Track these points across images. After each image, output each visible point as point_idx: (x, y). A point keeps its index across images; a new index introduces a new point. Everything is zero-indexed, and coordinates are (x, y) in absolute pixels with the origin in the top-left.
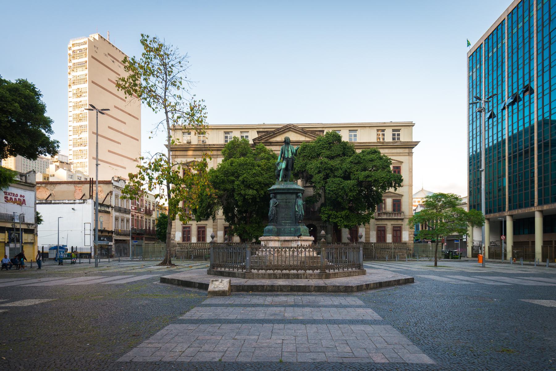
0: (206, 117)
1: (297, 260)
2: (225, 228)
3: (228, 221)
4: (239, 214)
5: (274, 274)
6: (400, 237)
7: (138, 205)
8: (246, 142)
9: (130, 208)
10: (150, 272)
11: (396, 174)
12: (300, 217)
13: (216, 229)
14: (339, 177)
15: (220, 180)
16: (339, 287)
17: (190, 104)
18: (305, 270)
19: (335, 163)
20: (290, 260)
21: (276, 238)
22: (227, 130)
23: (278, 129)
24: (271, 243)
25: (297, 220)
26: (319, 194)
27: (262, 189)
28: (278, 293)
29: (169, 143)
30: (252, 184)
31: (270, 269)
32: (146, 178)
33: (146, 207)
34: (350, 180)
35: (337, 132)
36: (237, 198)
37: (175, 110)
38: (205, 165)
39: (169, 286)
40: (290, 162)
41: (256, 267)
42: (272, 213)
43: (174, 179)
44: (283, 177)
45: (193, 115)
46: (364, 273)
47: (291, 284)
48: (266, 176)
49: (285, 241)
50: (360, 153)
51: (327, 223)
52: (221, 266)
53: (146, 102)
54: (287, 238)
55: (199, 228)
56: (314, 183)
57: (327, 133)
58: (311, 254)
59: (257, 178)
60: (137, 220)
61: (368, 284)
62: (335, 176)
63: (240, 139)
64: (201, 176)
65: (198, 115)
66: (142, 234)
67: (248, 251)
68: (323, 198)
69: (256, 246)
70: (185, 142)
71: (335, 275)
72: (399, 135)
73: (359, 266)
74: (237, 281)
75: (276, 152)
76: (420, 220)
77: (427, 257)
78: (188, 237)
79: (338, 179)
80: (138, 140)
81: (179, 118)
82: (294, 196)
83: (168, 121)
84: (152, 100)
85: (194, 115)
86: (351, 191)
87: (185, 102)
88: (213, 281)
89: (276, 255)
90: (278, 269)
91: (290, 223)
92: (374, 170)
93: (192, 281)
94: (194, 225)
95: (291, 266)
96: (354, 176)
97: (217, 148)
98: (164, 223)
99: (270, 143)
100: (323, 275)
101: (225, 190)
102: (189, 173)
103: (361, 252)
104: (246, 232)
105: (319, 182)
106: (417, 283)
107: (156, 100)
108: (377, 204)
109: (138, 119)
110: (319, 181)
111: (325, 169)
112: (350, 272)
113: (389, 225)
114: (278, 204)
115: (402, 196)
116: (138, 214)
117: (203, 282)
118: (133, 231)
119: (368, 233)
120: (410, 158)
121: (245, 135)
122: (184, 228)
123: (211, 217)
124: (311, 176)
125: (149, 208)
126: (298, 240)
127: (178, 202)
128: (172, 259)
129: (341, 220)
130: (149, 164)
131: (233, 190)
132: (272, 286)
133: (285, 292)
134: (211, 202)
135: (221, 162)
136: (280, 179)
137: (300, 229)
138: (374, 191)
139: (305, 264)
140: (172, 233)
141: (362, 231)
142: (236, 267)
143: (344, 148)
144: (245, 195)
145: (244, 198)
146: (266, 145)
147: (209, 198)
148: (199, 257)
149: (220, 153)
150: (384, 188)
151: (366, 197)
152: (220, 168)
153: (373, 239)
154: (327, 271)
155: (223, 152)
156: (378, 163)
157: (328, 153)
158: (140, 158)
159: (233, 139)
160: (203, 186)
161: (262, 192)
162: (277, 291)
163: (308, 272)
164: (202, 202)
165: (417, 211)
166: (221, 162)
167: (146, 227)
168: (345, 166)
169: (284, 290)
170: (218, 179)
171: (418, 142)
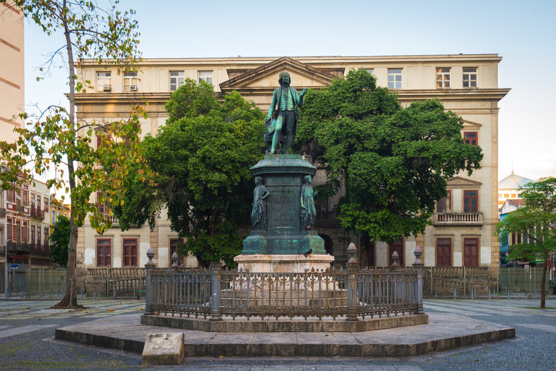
0: (138, 42)
1: (306, 298)
2: (172, 241)
3: (177, 230)
4: (198, 217)
5: (264, 324)
6: (477, 257)
7: (19, 201)
8: (207, 88)
9: (5, 207)
10: (39, 320)
11: (471, 146)
12: (308, 219)
13: (156, 242)
14: (371, 150)
15: (165, 157)
16: (383, 346)
17: (109, 18)
18: (320, 316)
19: (365, 125)
20: (291, 298)
21: (266, 257)
22: (174, 68)
23: (264, 66)
24: (257, 268)
25: (302, 225)
26: (336, 180)
27: (237, 172)
28: (272, 359)
29: (72, 88)
30: (219, 163)
31: (255, 315)
32: (32, 149)
33: (33, 206)
34: (392, 155)
35: (368, 71)
36: (192, 188)
37: (83, 29)
38: (136, 127)
39: (70, 346)
40: (290, 118)
41: (230, 312)
42: (258, 211)
43: (81, 154)
44: (277, 147)
45: (115, 38)
46: (424, 321)
47: (295, 342)
48: (244, 148)
49: (281, 262)
50: (408, 109)
51: (351, 232)
52: (166, 310)
53: (30, 15)
54: (286, 257)
55: (125, 241)
56: (327, 161)
57: (350, 72)
58: (331, 287)
59: (228, 151)
60: (17, 228)
61: (437, 342)
62: (365, 149)
63: (198, 84)
64: (129, 147)
65: (124, 38)
66: (27, 253)
67: (216, 280)
68: (343, 188)
69: (227, 272)
70: (101, 89)
71: (374, 325)
72: (474, 77)
73: (416, 309)
74: (196, 337)
75: (261, 107)
76: (517, 225)
77: (523, 291)
78: (106, 258)
79: (370, 154)
80: (18, 87)
81: (89, 42)
82: (298, 181)
83: (69, 49)
84: (41, 12)
85: (116, 38)
86: (393, 175)
87: (101, 14)
88: (151, 337)
89: (266, 288)
90: (270, 315)
91: (290, 230)
92: (433, 139)
93: (113, 336)
94: (117, 237)
95: (294, 308)
96: (398, 149)
97: (158, 100)
98: (65, 232)
100: (352, 324)
101: (171, 173)
102: (108, 142)
103: (420, 283)
104: (209, 248)
105: (337, 160)
106: (520, 338)
107: (48, 12)
108: (438, 198)
109: (18, 50)
110: (336, 157)
111: (347, 137)
112: (401, 319)
113: (458, 237)
114: (269, 196)
115: (480, 184)
116: (19, 217)
117: (134, 339)
118: (11, 248)
119: (419, 250)
120: (494, 118)
121: (204, 76)
122: (99, 241)
123: (147, 223)
124: (323, 150)
125: (39, 207)
126: (305, 262)
127: (88, 194)
128: (78, 296)
129: (375, 228)
130: (37, 125)
131: (186, 174)
132: (261, 346)
133: (284, 356)
134: (147, 195)
135: (164, 125)
136: (273, 150)
137: (308, 241)
138: (431, 176)
139: (319, 304)
140: (78, 250)
141: (410, 246)
142: (193, 311)
143: (381, 100)
144: (208, 182)
145: (206, 188)
146: (243, 95)
147: (143, 188)
148: (126, 293)
149: (162, 108)
150: (450, 171)
151: (419, 186)
152: (163, 135)
153: (430, 260)
154: (360, 318)
155: (167, 107)
156: (439, 126)
157: (352, 107)
158: (21, 116)
159: (185, 83)
160: (133, 165)
161: (237, 177)
162: (271, 355)
163: (325, 319)
164: (130, 194)
165: (503, 212)
166: (164, 125)
167: (33, 240)
168: (382, 131)
169: (283, 352)
170: (159, 154)
171: (507, 90)
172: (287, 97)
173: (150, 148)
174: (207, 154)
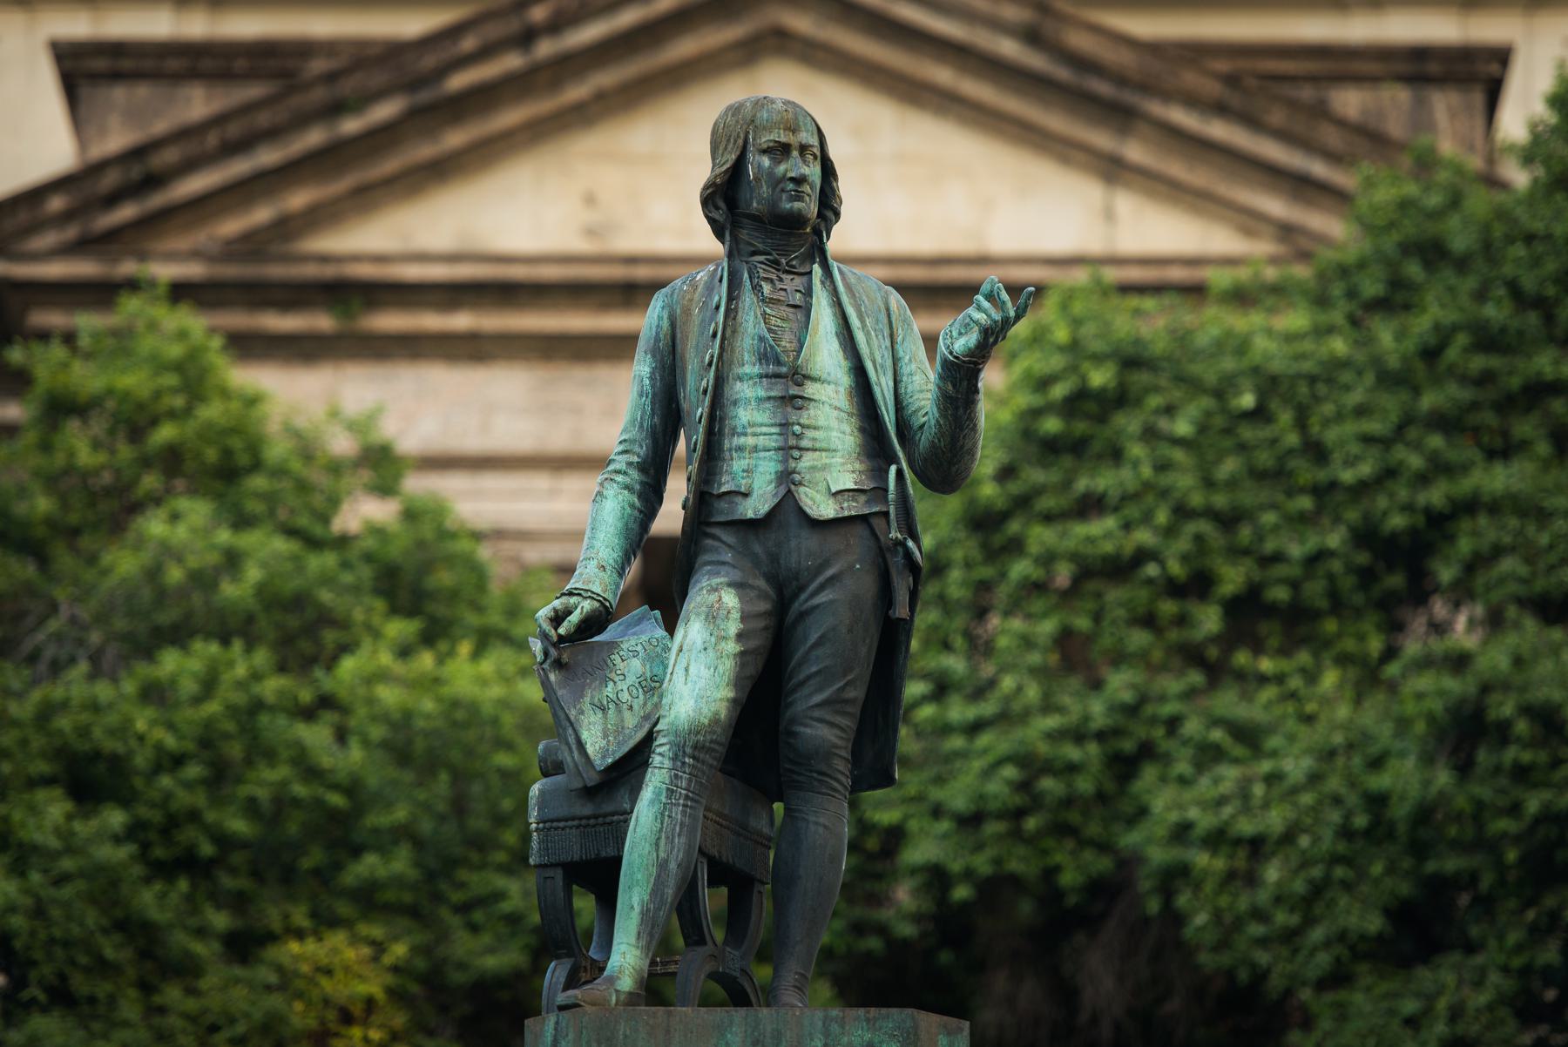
40: (837, 602)
99: (351, 293)
136: (626, 957)
146: (247, 346)
172: (798, 376)
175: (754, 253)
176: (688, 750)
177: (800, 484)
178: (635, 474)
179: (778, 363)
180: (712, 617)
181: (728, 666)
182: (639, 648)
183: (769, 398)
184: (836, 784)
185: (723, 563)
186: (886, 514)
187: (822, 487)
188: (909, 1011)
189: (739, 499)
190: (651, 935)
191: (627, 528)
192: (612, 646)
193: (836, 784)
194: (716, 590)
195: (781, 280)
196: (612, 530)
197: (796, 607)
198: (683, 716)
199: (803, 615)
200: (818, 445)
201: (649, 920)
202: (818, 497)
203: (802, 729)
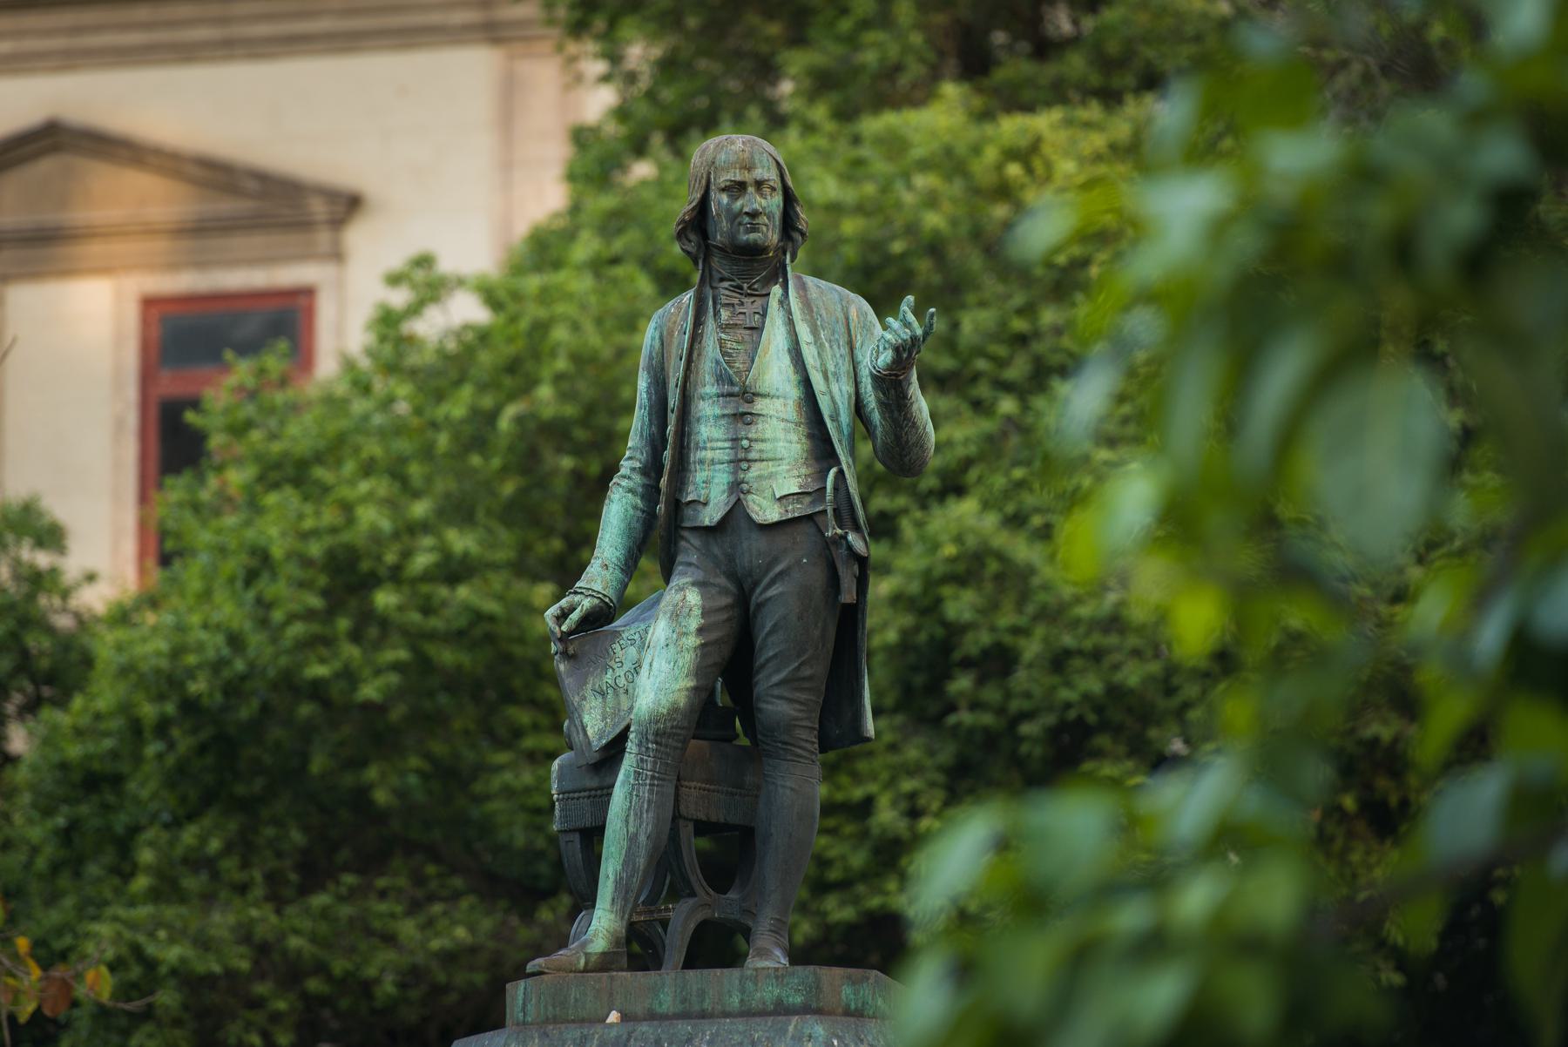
172: (748, 395)
173: (260, 563)
174: (960, 605)
175: (722, 280)
176: (651, 737)
177: (749, 492)
178: (637, 478)
179: (732, 383)
180: (676, 616)
181: (688, 659)
182: (636, 637)
183: (724, 416)
184: (800, 751)
185: (690, 564)
186: (824, 512)
187: (768, 493)
188: (811, 968)
189: (700, 507)
190: (625, 899)
191: (630, 528)
192: (616, 634)
193: (800, 751)
194: (682, 589)
195: (742, 304)
196: (615, 531)
197: (754, 600)
198: (644, 708)
199: (760, 606)
200: (764, 456)
201: (622, 887)
202: (765, 503)
203: (764, 706)
